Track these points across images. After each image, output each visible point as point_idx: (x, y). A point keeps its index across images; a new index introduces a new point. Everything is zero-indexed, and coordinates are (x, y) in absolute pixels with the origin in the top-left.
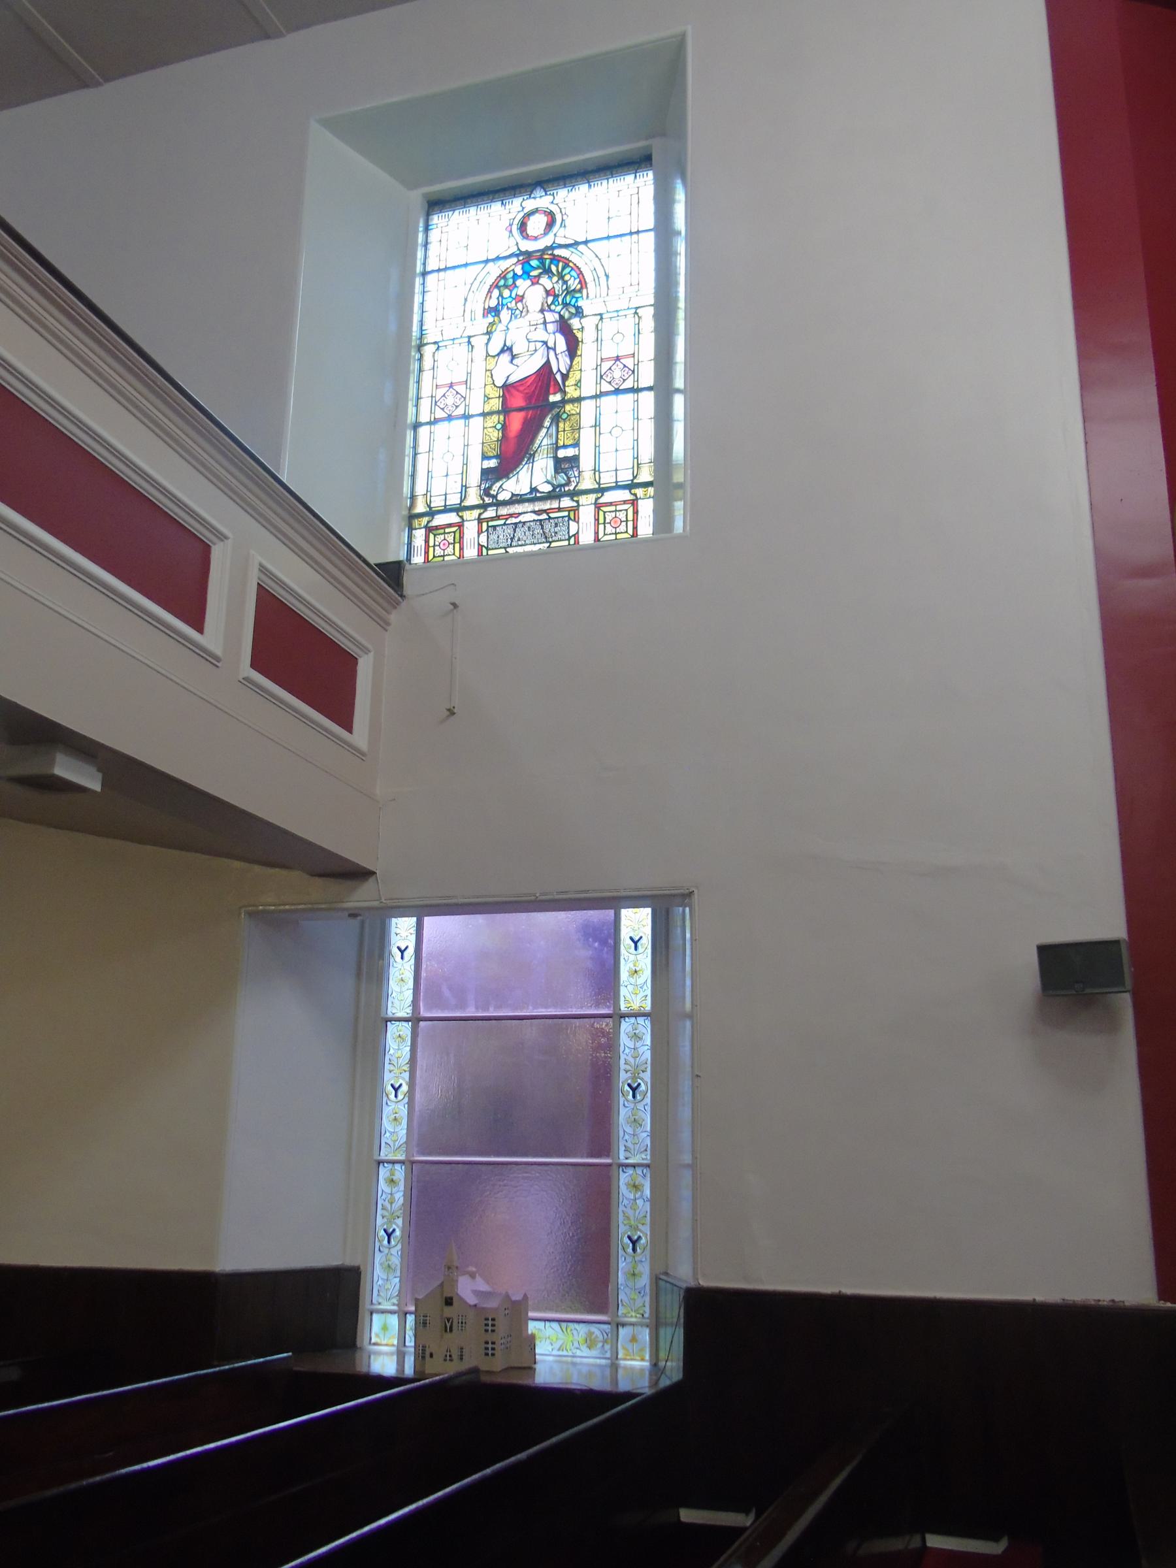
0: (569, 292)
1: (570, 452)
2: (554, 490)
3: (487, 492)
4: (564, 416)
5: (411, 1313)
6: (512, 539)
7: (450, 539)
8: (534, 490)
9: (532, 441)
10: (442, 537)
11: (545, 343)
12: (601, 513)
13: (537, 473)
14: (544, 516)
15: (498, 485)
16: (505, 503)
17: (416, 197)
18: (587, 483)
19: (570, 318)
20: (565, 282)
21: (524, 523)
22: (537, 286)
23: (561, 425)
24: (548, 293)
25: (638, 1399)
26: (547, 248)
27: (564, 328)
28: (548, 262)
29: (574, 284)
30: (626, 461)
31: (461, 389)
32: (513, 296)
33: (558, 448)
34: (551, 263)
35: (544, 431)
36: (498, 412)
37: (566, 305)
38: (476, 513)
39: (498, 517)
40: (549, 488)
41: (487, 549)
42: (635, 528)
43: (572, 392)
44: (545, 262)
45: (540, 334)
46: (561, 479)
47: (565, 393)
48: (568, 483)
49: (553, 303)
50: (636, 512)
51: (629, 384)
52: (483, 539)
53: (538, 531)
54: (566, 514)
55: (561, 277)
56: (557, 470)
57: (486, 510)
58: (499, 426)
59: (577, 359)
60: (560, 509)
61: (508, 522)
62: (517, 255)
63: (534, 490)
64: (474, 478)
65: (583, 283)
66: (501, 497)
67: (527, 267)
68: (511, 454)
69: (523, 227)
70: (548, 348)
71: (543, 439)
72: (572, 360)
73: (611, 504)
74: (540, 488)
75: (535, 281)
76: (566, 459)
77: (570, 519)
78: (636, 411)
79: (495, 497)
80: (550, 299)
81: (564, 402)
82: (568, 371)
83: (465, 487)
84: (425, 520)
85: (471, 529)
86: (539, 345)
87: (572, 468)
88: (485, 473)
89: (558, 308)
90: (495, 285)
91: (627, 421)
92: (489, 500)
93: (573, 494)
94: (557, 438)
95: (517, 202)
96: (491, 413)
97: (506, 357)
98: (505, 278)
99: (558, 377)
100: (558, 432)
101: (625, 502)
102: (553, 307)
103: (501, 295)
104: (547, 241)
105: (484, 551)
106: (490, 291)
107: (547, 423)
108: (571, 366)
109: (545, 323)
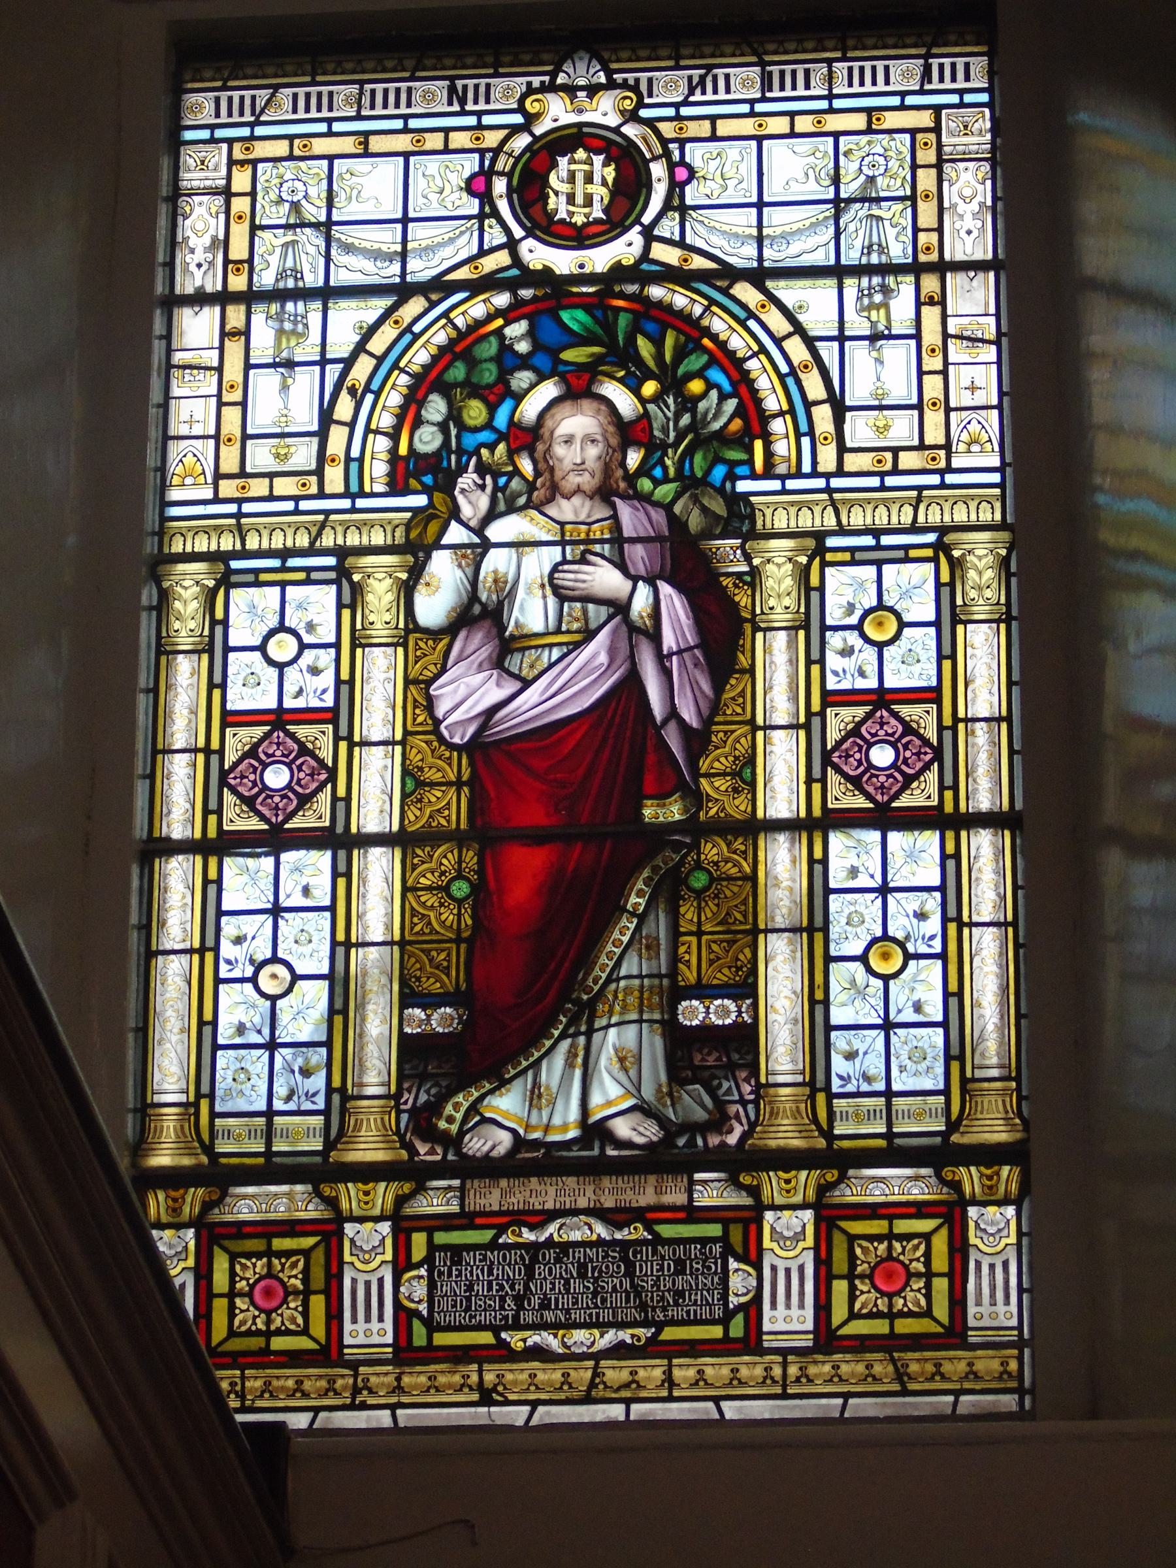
0: (702, 438)
1: (722, 1012)
3: (423, 1122)
4: (699, 880)
6: (519, 1299)
9: (586, 956)
12: (839, 1241)
13: (601, 1081)
14: (637, 1232)
15: (463, 1100)
18: (786, 1134)
19: (707, 534)
20: (689, 403)
21: (566, 1247)
23: (688, 912)
25: (138, 1204)
26: (618, 272)
27: (684, 561)
28: (623, 321)
29: (721, 414)
30: (919, 1066)
33: (677, 993)
34: (635, 329)
36: (457, 838)
37: (690, 484)
38: (383, 1195)
39: (466, 1219)
40: (650, 1132)
41: (432, 1327)
42: (958, 1301)
44: (621, 328)
45: (605, 578)
46: (694, 1104)
47: (696, 798)
48: (719, 1121)
49: (644, 470)
50: (959, 1249)
52: (416, 1289)
54: (715, 1230)
55: (673, 383)
57: (420, 1189)
58: (461, 889)
59: (734, 686)
60: (692, 1213)
61: (508, 1238)
62: (511, 285)
63: (595, 1131)
64: (376, 1070)
66: (476, 1145)
67: (550, 333)
69: (530, 188)
70: (633, 629)
71: (623, 958)
72: (719, 686)
74: (623, 1128)
75: (578, 388)
76: (707, 1032)
78: (951, 888)
79: (454, 1142)
81: (697, 829)
82: (708, 722)
84: (193, 1198)
85: (368, 1241)
88: (413, 1052)
90: (425, 383)
91: (916, 920)
92: (428, 1149)
93: (743, 1163)
94: (675, 959)
95: (507, 89)
96: (430, 837)
97: (475, 645)
99: (673, 739)
100: (675, 934)
101: (919, 1210)
103: (454, 415)
104: (624, 249)
106: (414, 401)
107: (636, 901)
108: (716, 706)
109: (618, 540)
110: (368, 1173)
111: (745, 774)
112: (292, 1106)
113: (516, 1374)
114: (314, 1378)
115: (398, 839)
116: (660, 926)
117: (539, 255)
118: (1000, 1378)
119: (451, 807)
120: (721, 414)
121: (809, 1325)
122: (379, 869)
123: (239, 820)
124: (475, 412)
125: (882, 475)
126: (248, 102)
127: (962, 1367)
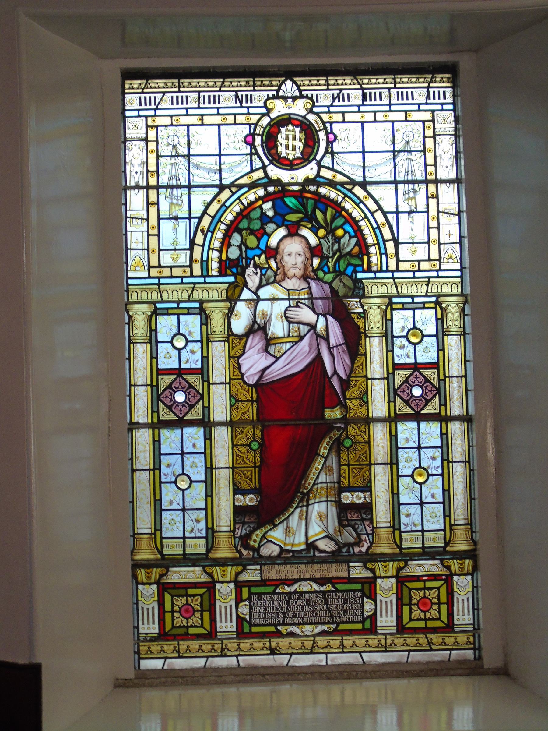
1: (358, 498)
2: (339, 550)
4: (348, 443)
5: (363, 626)
7: (196, 603)
8: (311, 546)
9: (304, 474)
10: (184, 600)
11: (313, 327)
13: (311, 524)
15: (259, 533)
16: (271, 560)
17: (113, 68)
21: (301, 593)
22: (296, 239)
23: (344, 455)
24: (315, 251)
27: (338, 309)
28: (311, 203)
29: (349, 244)
30: (434, 520)
31: (195, 380)
32: (263, 246)
35: (319, 463)
37: (339, 274)
38: (230, 571)
42: (450, 614)
43: (355, 409)
45: (306, 314)
46: (348, 536)
47: (345, 408)
48: (358, 542)
49: (320, 268)
50: (450, 593)
51: (432, 408)
52: (244, 609)
53: (321, 606)
54: (358, 586)
55: (331, 231)
56: (343, 522)
57: (245, 569)
58: (255, 445)
59: (359, 360)
60: (350, 580)
63: (311, 546)
64: (224, 519)
65: (363, 247)
66: (265, 551)
68: (274, 488)
69: (270, 141)
70: (318, 336)
71: (321, 473)
73: (418, 578)
75: (293, 231)
77: (364, 595)
79: (257, 550)
80: (316, 262)
82: (349, 376)
83: (211, 532)
84: (155, 573)
85: (225, 591)
86: (304, 329)
87: (363, 520)
88: (239, 512)
89: (329, 277)
90: (233, 228)
91: (432, 460)
92: (247, 552)
98: (248, 217)
99: (335, 382)
100: (340, 465)
102: (320, 274)
103: (243, 243)
105: (246, 625)
106: (227, 235)
107: (323, 451)
108: (352, 371)
110: (223, 563)
111: (364, 398)
112: (193, 535)
113: (283, 643)
114: (206, 645)
115: (231, 424)
116: (333, 461)
117: (275, 172)
118: (467, 644)
119: (250, 411)
120: (349, 244)
121: (235, 629)
122: (222, 435)
123: (403, 409)
124: (252, 241)
125: (414, 272)
126: (249, 97)
127: (452, 640)
